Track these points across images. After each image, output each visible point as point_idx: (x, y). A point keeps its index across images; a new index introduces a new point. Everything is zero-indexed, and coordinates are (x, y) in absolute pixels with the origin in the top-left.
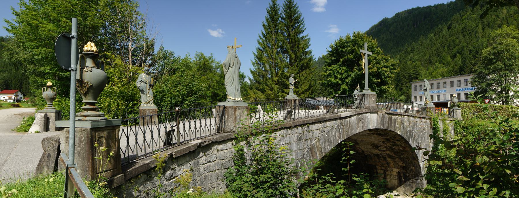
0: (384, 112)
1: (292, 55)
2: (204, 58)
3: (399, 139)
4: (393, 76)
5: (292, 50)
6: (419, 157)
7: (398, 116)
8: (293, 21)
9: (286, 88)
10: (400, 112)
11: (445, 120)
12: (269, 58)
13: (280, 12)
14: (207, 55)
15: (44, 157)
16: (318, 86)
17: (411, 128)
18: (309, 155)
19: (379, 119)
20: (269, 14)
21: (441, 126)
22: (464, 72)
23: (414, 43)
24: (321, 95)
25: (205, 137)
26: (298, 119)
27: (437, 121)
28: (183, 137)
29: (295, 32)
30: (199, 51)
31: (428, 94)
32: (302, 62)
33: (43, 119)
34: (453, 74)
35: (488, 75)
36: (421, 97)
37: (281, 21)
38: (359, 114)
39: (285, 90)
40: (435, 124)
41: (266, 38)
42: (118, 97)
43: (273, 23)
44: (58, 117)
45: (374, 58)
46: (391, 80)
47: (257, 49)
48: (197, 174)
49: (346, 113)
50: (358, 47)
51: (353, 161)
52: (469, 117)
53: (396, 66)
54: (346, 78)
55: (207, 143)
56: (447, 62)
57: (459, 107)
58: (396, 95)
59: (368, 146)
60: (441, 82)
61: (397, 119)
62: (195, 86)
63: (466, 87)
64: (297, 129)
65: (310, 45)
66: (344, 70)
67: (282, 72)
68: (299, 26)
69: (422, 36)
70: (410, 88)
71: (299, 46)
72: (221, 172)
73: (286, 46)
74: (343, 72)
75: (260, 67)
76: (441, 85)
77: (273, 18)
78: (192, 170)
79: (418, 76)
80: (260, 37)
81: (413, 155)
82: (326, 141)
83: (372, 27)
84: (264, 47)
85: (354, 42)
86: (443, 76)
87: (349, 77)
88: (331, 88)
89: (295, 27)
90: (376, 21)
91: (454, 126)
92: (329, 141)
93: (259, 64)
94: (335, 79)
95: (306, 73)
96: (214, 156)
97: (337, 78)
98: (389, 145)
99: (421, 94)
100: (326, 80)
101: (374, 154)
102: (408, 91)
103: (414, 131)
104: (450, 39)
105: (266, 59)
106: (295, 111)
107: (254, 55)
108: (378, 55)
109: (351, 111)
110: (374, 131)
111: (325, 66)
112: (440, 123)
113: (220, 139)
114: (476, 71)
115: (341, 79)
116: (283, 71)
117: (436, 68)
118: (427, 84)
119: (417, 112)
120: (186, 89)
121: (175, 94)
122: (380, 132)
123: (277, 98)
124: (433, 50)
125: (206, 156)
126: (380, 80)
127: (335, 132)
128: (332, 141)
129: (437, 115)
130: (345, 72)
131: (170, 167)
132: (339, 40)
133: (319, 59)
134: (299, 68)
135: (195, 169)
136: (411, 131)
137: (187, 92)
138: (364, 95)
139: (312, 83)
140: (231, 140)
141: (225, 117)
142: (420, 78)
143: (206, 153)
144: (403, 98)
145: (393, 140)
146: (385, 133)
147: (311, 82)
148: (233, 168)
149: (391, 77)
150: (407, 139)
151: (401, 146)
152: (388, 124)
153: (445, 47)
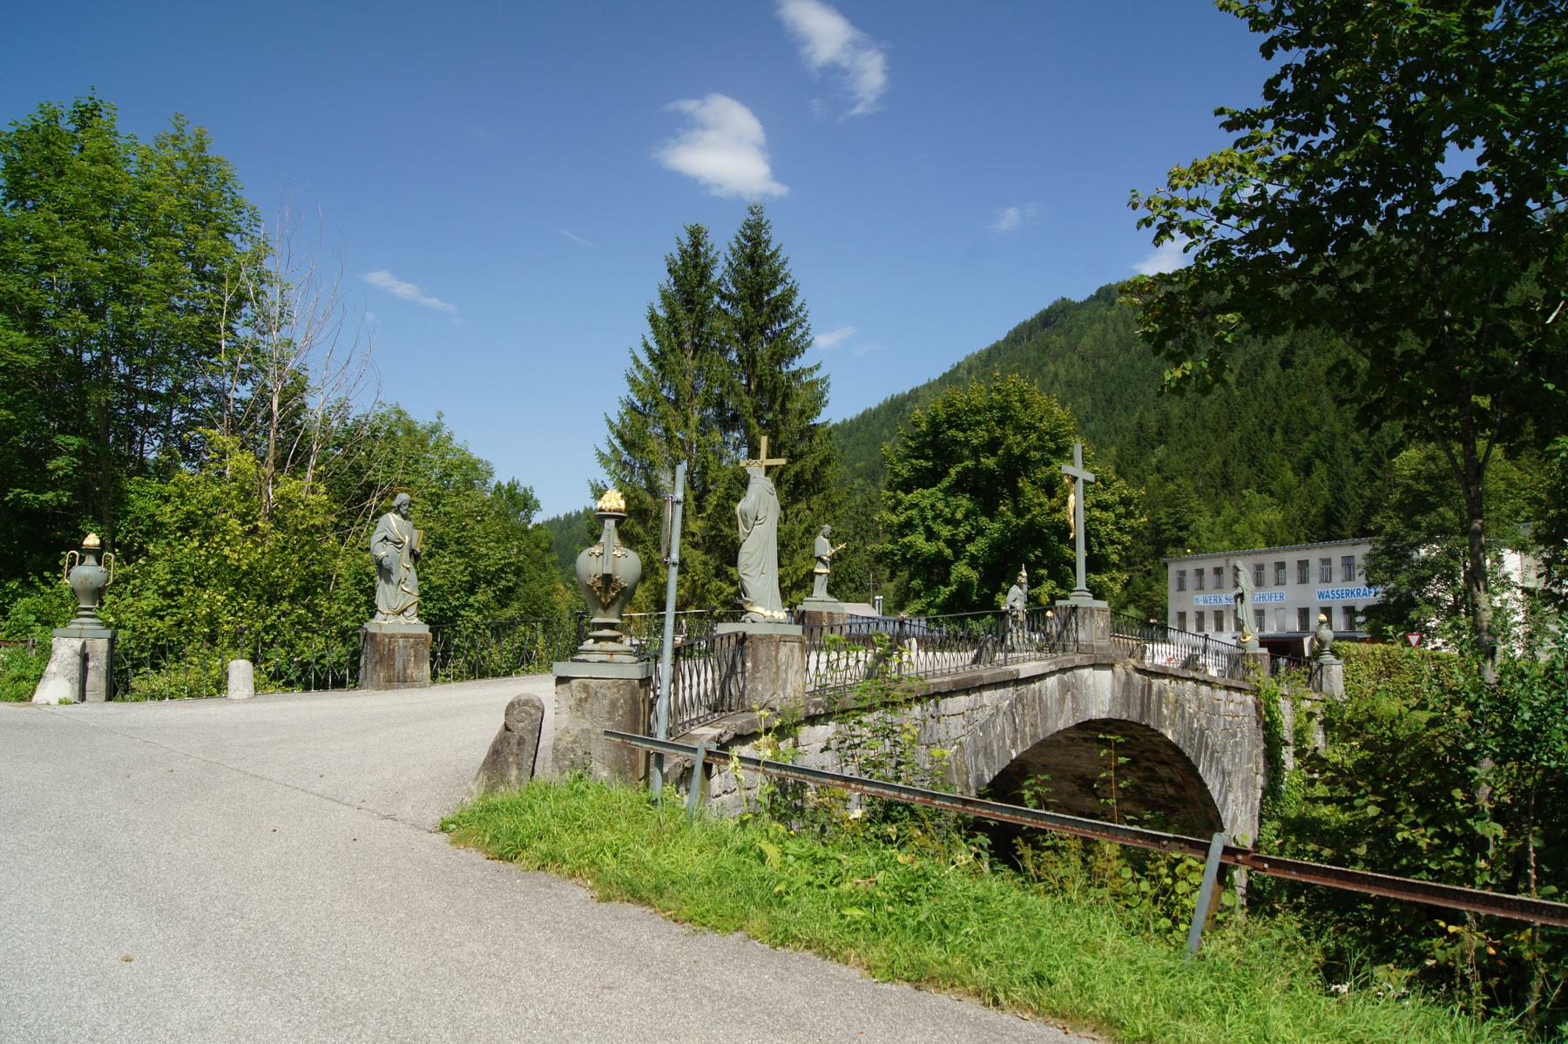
3: (1167, 759)
7: (1167, 681)
13: (716, 274)
22: (1341, 527)
27: (1275, 702)
34: (1303, 532)
35: (1415, 546)
38: (1063, 671)
40: (1269, 713)
41: (661, 367)
46: (1120, 555)
52: (1365, 690)
53: (1137, 506)
54: (970, 538)
56: (1284, 488)
57: (1338, 657)
60: (1270, 560)
61: (1166, 691)
63: (1351, 586)
66: (962, 510)
68: (790, 330)
71: (789, 406)
74: (959, 516)
79: (1183, 534)
80: (635, 359)
81: (1207, 813)
83: (1016, 331)
90: (1029, 310)
92: (987, 751)
94: (928, 540)
95: (811, 510)
100: (894, 542)
102: (1150, 588)
107: (611, 428)
111: (890, 487)
114: (1379, 530)
115: (951, 543)
117: (1246, 506)
124: (1234, 436)
128: (996, 754)
130: (966, 517)
136: (1202, 733)
138: (1075, 609)
145: (1148, 760)
151: (1171, 781)
152: (1142, 705)
153: (1274, 430)
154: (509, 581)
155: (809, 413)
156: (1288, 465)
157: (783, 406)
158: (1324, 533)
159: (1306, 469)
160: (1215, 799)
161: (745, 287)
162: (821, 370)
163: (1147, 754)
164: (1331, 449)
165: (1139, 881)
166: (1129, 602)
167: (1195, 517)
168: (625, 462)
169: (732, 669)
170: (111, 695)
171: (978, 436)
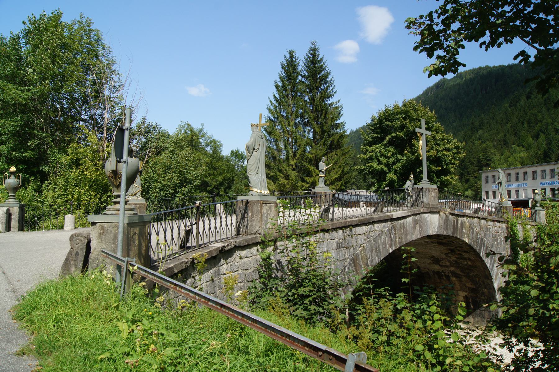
0: (447, 212)
1: (316, 128)
2: (192, 131)
4: (457, 162)
5: (317, 122)
6: (493, 274)
7: (465, 218)
8: (318, 80)
9: (307, 176)
10: (469, 213)
11: (526, 225)
12: (283, 132)
13: (299, 68)
14: (196, 126)
15: (71, 255)
16: (354, 173)
17: (483, 235)
18: (352, 267)
19: (441, 222)
20: (285, 71)
21: (521, 232)
22: (550, 158)
23: (483, 115)
24: (354, 186)
25: (225, 239)
26: (337, 219)
28: (203, 238)
29: (321, 97)
30: (185, 121)
31: (504, 189)
32: (331, 139)
33: (5, 215)
34: (535, 161)
36: (494, 193)
37: (301, 81)
38: (415, 215)
39: (306, 178)
40: (512, 231)
41: (279, 104)
42: (91, 186)
43: (290, 82)
44: (21, 212)
45: (432, 137)
46: (455, 168)
47: (266, 118)
48: (217, 286)
49: (399, 212)
50: (410, 121)
51: (415, 270)
54: (394, 163)
55: (229, 247)
56: (528, 144)
57: (543, 208)
58: (460, 189)
59: (426, 260)
60: (521, 171)
61: (465, 222)
62: (190, 173)
64: (337, 232)
65: (343, 114)
67: (302, 153)
68: (327, 88)
69: (493, 106)
70: (480, 180)
71: (328, 116)
72: (244, 286)
73: (309, 115)
74: (389, 155)
75: (271, 144)
76: (521, 176)
77: (289, 76)
78: (212, 280)
79: (489, 162)
80: (271, 101)
82: (373, 250)
83: (426, 90)
84: (276, 116)
85: (405, 114)
86: (523, 164)
87: (397, 162)
88: (373, 178)
89: (322, 89)
91: (537, 233)
92: (377, 250)
93: (268, 140)
94: (378, 165)
95: (337, 155)
96: (237, 264)
97: (382, 164)
98: (454, 258)
99: (495, 188)
101: (434, 272)
102: (476, 183)
103: (487, 239)
104: (530, 112)
105: (278, 133)
106: (333, 209)
108: (437, 133)
109: (405, 210)
110: (435, 238)
111: (365, 145)
112: (520, 229)
113: (243, 243)
115: (387, 165)
116: (304, 150)
117: (513, 151)
118: (502, 176)
119: (490, 213)
120: (179, 177)
121: (166, 183)
122: (442, 240)
123: (295, 189)
124: (509, 125)
125: (227, 263)
126: (440, 168)
127: (385, 238)
128: (381, 250)
129: (516, 218)
130: (393, 155)
131: (191, 275)
132: (384, 109)
133: (352, 132)
134: (326, 147)
135: (215, 279)
137: (180, 180)
138: (422, 189)
139: (346, 169)
140: (256, 244)
141: (248, 214)
142: (492, 165)
143: (228, 260)
144: (470, 194)
145: (459, 251)
146: (448, 241)
147: (344, 167)
148: (258, 281)
149: (454, 164)
150: (477, 250)
152: (454, 228)
153: (524, 123)
154: (198, 182)
155: (335, 118)
156: (529, 136)
157: (325, 116)
158: (543, 161)
159: (537, 137)
160: (488, 267)
161: (310, 72)
162: (340, 102)
163: (458, 248)
164: (547, 129)
165: (415, 322)
166: (469, 188)
167: (493, 156)
168: (268, 140)
169: (243, 218)
170: (21, 229)
171: (397, 124)
